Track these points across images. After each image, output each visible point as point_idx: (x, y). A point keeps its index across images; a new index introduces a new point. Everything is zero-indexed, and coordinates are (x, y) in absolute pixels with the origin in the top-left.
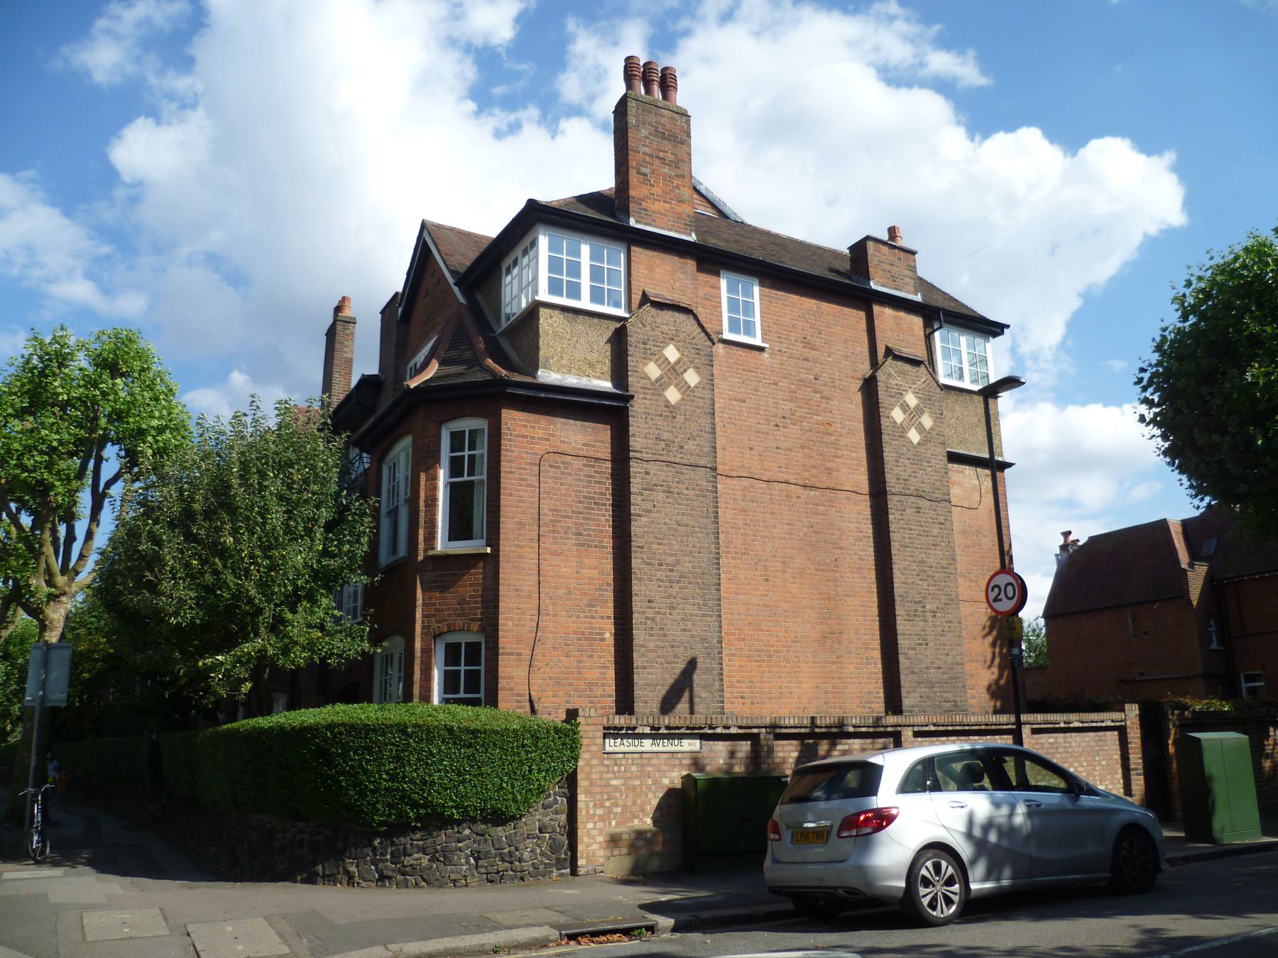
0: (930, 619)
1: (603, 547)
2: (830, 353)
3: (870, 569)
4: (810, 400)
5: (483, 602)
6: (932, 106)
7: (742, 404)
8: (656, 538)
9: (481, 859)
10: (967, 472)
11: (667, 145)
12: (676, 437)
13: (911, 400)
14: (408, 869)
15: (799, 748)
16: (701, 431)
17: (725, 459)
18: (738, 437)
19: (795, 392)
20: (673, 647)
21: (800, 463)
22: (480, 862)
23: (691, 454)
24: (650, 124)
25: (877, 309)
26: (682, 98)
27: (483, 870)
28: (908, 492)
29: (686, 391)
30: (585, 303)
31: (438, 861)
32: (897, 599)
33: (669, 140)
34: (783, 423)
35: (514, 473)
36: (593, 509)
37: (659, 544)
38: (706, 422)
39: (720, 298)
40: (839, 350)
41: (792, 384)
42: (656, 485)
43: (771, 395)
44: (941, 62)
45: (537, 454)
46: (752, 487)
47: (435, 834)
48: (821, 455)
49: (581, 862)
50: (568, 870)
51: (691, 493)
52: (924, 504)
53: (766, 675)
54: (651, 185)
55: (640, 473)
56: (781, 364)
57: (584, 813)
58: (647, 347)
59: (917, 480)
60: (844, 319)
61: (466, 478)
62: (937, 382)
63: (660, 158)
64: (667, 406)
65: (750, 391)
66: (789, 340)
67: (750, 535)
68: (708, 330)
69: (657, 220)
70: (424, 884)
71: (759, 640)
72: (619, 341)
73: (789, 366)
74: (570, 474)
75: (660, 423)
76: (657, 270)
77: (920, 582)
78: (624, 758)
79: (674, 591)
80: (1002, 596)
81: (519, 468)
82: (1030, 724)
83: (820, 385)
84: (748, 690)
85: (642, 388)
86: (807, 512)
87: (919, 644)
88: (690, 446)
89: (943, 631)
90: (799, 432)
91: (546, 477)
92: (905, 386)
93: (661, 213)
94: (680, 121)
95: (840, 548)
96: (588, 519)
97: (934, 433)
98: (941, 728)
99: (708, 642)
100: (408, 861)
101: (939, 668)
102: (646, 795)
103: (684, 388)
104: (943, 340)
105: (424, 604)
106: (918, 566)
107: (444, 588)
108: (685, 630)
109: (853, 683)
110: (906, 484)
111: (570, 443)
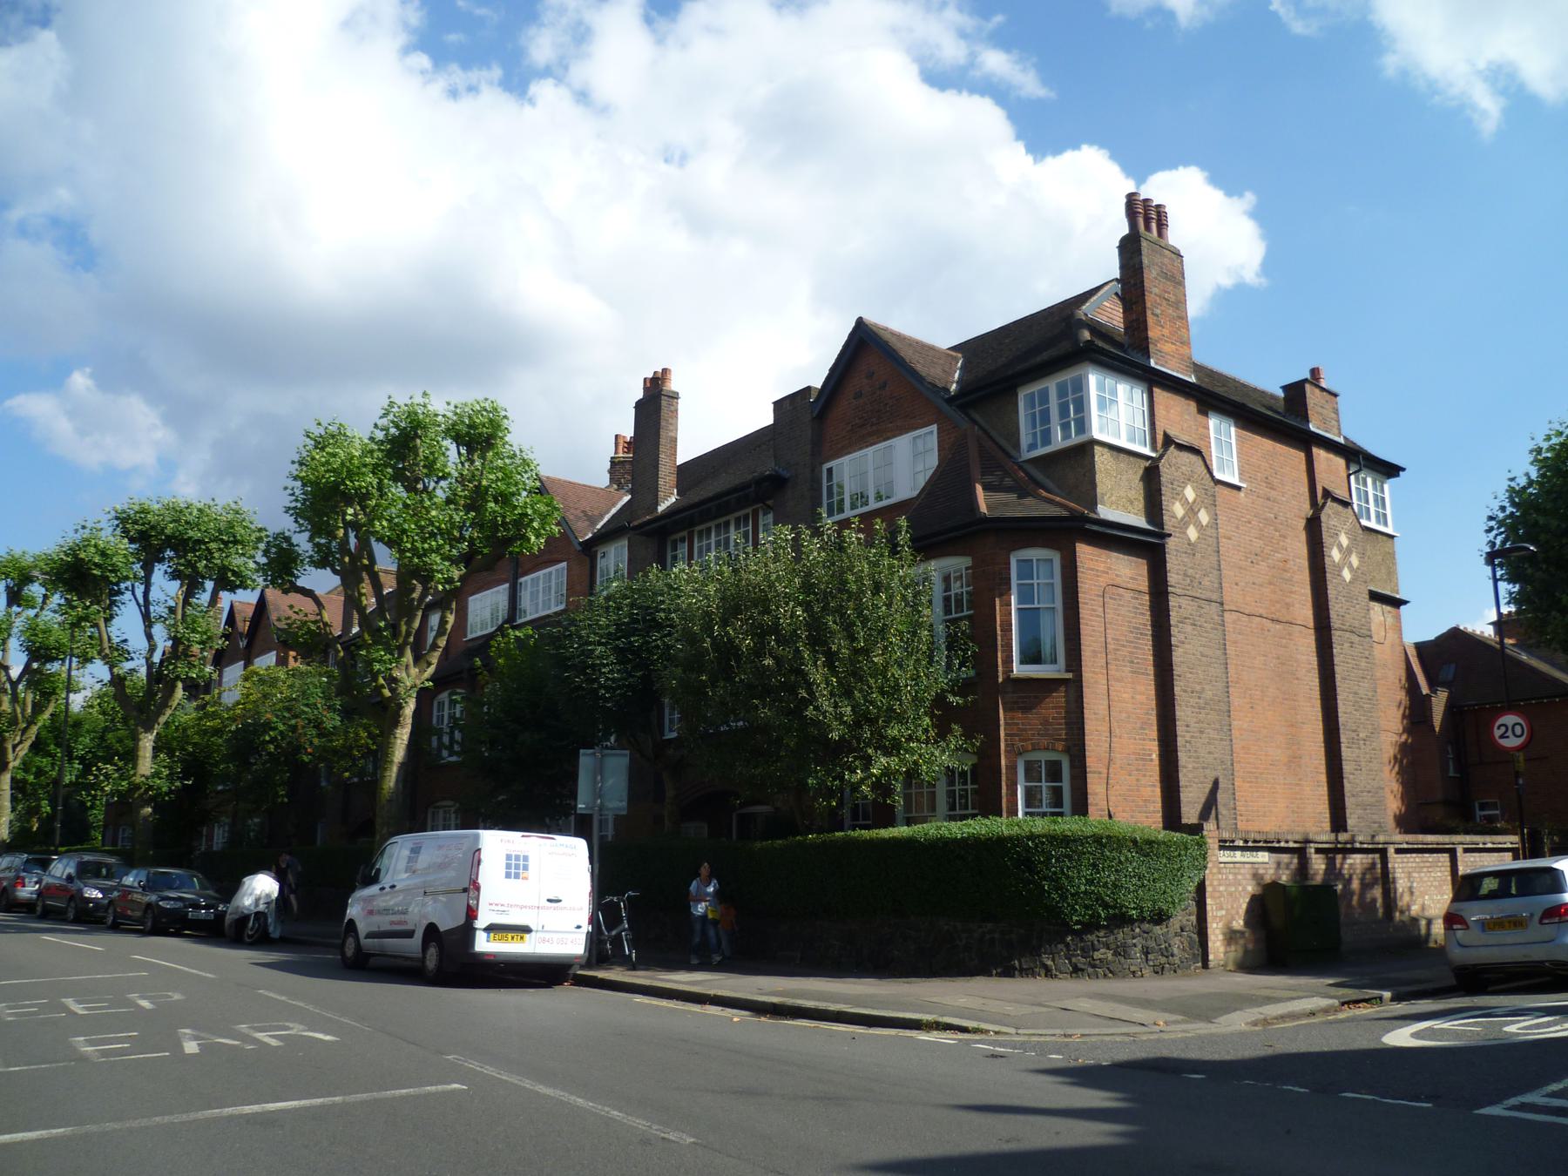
3: (1316, 699)
4: (1272, 538)
5: (1066, 724)
6: (986, 116)
7: (1229, 541)
9: (1149, 953)
14: (1098, 962)
15: (1325, 861)
17: (1232, 596)
22: (1150, 956)
27: (1151, 963)
28: (1344, 627)
31: (1120, 954)
32: (1341, 727)
37: (1191, 673)
38: (1214, 559)
41: (1260, 522)
42: (1185, 618)
44: (995, 62)
46: (1239, 620)
47: (1116, 931)
48: (1281, 590)
49: (1211, 957)
50: (1200, 964)
51: (1208, 626)
52: (1356, 639)
61: (1036, 605)
62: (1360, 523)
63: (1166, 299)
64: (1189, 544)
70: (1110, 975)
72: (1152, 477)
79: (1202, 716)
80: (1509, 733)
98: (1410, 846)
100: (1097, 955)
101: (1369, 792)
105: (1006, 724)
107: (1027, 709)
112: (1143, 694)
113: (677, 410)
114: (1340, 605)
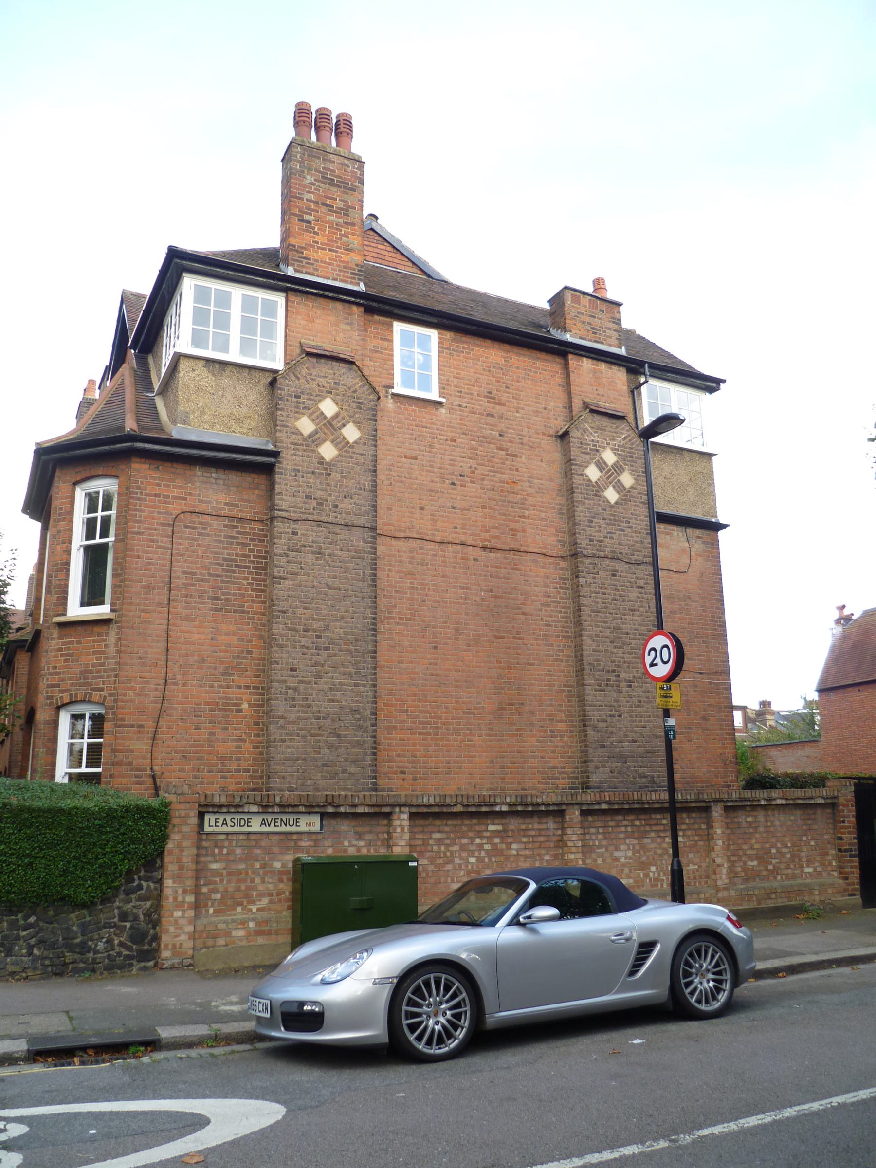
0: (625, 689)
1: (243, 612)
2: (518, 408)
4: (493, 457)
8: (302, 602)
10: (675, 534)
11: (336, 192)
12: (330, 495)
13: (609, 457)
16: (360, 489)
18: (407, 496)
19: (475, 449)
20: (319, 718)
21: (479, 524)
23: (348, 513)
24: (317, 170)
25: (573, 360)
26: (358, 146)
28: (603, 554)
29: (344, 447)
30: (234, 356)
33: (338, 186)
34: (460, 481)
35: (143, 534)
36: (234, 572)
37: (305, 608)
39: (392, 350)
40: (529, 405)
43: (447, 452)
45: (171, 514)
48: (504, 515)
51: (345, 555)
52: (620, 566)
53: (432, 748)
54: (314, 233)
55: (286, 533)
56: (461, 420)
57: (171, 900)
58: (301, 400)
59: (613, 541)
60: (536, 373)
64: (321, 463)
65: (423, 448)
66: (471, 394)
67: (417, 600)
68: (374, 384)
69: (320, 269)
71: (424, 712)
73: (470, 421)
74: (208, 535)
75: (312, 481)
76: (318, 321)
77: (614, 650)
78: (227, 839)
80: (658, 660)
81: (149, 529)
82: (410, 806)
83: (505, 442)
84: (410, 765)
85: (292, 444)
86: (486, 576)
87: (611, 716)
88: (346, 505)
89: (640, 702)
90: (480, 490)
91: (179, 538)
92: (602, 443)
93: (325, 262)
94: (352, 167)
95: (524, 614)
96: (227, 582)
97: (636, 491)
99: (359, 714)
101: (634, 741)
102: (253, 881)
103: (341, 443)
104: (201, 295)
106: (612, 632)
108: (333, 701)
109: (534, 757)
110: (601, 546)
111: (210, 502)
112: (234, 634)
114: (597, 529)
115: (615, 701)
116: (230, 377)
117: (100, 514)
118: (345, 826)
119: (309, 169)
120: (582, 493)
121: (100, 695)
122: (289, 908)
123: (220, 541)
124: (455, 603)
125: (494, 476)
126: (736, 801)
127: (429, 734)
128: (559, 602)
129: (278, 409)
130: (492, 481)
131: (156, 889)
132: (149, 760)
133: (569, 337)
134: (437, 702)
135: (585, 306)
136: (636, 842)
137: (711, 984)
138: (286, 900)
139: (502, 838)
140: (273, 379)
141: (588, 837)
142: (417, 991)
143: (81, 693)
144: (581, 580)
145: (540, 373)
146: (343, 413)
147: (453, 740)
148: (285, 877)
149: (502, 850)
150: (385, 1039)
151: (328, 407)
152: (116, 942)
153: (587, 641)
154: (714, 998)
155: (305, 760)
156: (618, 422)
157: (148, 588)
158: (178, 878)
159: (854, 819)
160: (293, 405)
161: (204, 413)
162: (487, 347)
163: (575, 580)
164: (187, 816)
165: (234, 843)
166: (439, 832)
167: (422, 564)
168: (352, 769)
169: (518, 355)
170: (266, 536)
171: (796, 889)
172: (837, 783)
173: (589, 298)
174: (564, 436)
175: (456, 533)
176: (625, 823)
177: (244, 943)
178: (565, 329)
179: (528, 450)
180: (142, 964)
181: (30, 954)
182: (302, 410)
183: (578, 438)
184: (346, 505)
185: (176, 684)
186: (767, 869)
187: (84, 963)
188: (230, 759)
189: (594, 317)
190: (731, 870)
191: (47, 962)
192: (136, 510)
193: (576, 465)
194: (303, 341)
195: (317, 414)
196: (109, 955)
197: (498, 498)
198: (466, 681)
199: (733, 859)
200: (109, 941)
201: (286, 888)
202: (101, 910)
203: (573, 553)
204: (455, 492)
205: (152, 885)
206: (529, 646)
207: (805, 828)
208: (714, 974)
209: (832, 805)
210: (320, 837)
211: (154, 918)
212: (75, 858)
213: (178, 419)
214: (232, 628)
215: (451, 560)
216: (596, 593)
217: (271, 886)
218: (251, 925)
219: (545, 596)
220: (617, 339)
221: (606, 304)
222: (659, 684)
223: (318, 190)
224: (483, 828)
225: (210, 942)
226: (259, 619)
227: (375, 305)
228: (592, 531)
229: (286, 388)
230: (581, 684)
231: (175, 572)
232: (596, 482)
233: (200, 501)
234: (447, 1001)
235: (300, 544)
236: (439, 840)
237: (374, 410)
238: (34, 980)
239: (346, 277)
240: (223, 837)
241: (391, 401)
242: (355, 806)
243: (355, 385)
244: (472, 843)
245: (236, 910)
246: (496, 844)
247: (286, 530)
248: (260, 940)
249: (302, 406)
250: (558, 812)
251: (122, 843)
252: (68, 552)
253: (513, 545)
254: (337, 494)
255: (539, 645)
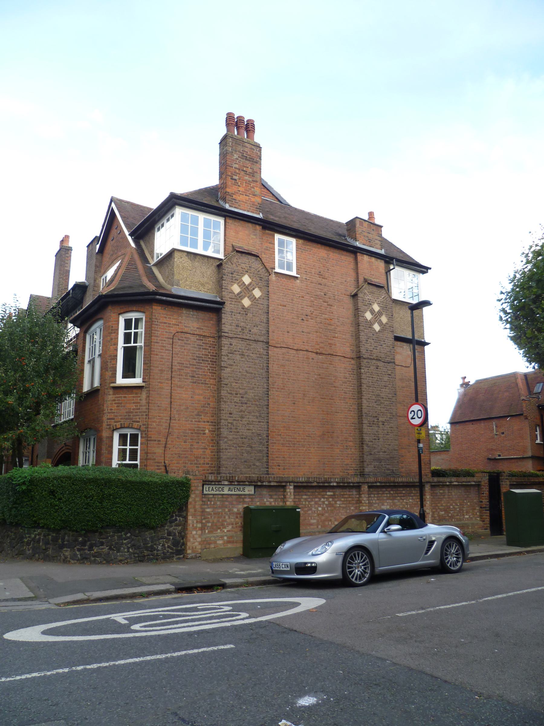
0: (381, 426)
1: (206, 384)
4: (321, 306)
8: (235, 380)
10: (405, 347)
11: (248, 164)
12: (247, 325)
13: (376, 308)
19: (313, 302)
23: (255, 334)
25: (360, 257)
26: (258, 138)
28: (372, 357)
30: (200, 250)
33: (249, 161)
34: (306, 318)
36: (201, 363)
37: (236, 383)
43: (300, 303)
45: (172, 333)
48: (326, 336)
51: (254, 356)
52: (380, 364)
54: (238, 186)
56: (306, 286)
57: (191, 526)
58: (234, 275)
64: (243, 308)
65: (288, 301)
66: (311, 273)
68: (267, 267)
71: (289, 436)
73: (310, 287)
74: (189, 344)
78: (213, 497)
80: (415, 416)
81: (161, 340)
84: (282, 462)
85: (230, 298)
86: (317, 367)
88: (255, 330)
91: (176, 345)
92: (373, 300)
93: (243, 202)
95: (335, 387)
97: (388, 325)
99: (261, 436)
101: (385, 452)
102: (225, 517)
103: (252, 298)
106: (376, 397)
108: (249, 430)
109: (339, 459)
110: (371, 353)
111: (189, 327)
112: (202, 395)
113: (70, 256)
114: (370, 344)
115: (377, 432)
116: (198, 262)
117: (133, 331)
118: (265, 492)
119: (236, 151)
120: (363, 326)
121: (138, 425)
122: (241, 530)
123: (195, 347)
124: (303, 381)
125: (321, 316)
126: (436, 482)
127: (291, 447)
128: (350, 381)
129: (223, 280)
130: (320, 318)
131: (183, 521)
132: (163, 458)
133: (358, 244)
134: (294, 431)
135: (366, 228)
136: (391, 501)
137: (455, 559)
138: (239, 527)
139: (333, 498)
140: (220, 265)
141: (370, 499)
142: (352, 558)
143: (127, 424)
144: (362, 371)
145: (344, 262)
146: (254, 283)
147: (302, 450)
148: (239, 516)
149: (333, 504)
150: (341, 577)
151: (246, 279)
152: (166, 546)
153: (364, 401)
154: (456, 565)
155: (236, 459)
156: (380, 289)
157: (162, 371)
158: (194, 515)
159: (488, 492)
160: (230, 278)
161: (186, 280)
162: (319, 248)
163: (359, 370)
164: (198, 486)
165: (216, 499)
166: (306, 495)
167: (288, 361)
168: (257, 464)
169: (333, 252)
170: (216, 345)
171: (461, 525)
172: (481, 475)
173: (367, 223)
174: (354, 296)
175: (304, 345)
176: (387, 492)
177: (222, 547)
178: (356, 239)
179: (337, 302)
180: (178, 556)
181: (128, 551)
182: (234, 281)
183: (362, 297)
184: (255, 330)
185: (175, 420)
186: (448, 516)
187: (152, 555)
188: (200, 458)
189: (370, 233)
190: (432, 516)
191: (136, 555)
192: (156, 330)
193: (361, 311)
194: (234, 244)
195: (241, 283)
196: (164, 552)
197: (323, 327)
198: (308, 421)
199: (434, 510)
200: (163, 545)
201: (240, 521)
202: (159, 531)
203: (358, 356)
204: (303, 324)
205: (181, 519)
206: (337, 403)
207: (465, 496)
208: (456, 555)
209: (478, 485)
210: (254, 497)
211: (183, 535)
212: (150, 505)
213: (175, 283)
214: (201, 392)
215: (302, 359)
216: (369, 377)
217: (232, 520)
218: (225, 538)
219: (344, 378)
220: (380, 245)
221: (375, 226)
222: (416, 428)
223: (240, 162)
224: (324, 493)
225: (208, 546)
226: (213, 387)
227: (268, 225)
228: (367, 346)
229: (227, 269)
230: (361, 423)
231: (174, 362)
232: (370, 321)
233: (185, 326)
234: (362, 563)
235: (233, 350)
236: (306, 499)
237: (268, 281)
238: (131, 564)
239: (254, 210)
240: (211, 496)
241: (274, 276)
242: (270, 482)
243: (259, 268)
244: (320, 501)
245: (217, 531)
246: (330, 501)
247: (227, 343)
248: (229, 546)
249: (234, 278)
250: (357, 487)
251: (170, 499)
252: (116, 350)
253: (330, 352)
254: (251, 325)
255: (341, 403)
